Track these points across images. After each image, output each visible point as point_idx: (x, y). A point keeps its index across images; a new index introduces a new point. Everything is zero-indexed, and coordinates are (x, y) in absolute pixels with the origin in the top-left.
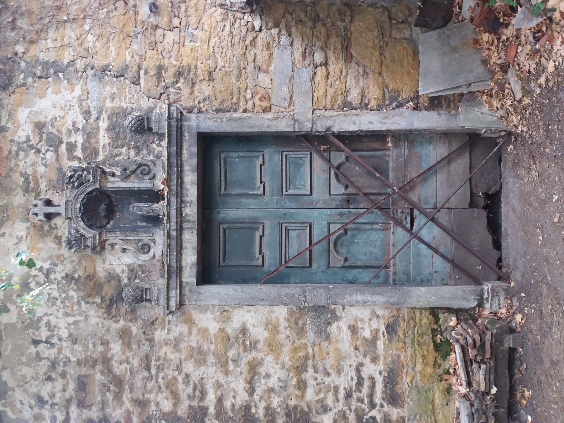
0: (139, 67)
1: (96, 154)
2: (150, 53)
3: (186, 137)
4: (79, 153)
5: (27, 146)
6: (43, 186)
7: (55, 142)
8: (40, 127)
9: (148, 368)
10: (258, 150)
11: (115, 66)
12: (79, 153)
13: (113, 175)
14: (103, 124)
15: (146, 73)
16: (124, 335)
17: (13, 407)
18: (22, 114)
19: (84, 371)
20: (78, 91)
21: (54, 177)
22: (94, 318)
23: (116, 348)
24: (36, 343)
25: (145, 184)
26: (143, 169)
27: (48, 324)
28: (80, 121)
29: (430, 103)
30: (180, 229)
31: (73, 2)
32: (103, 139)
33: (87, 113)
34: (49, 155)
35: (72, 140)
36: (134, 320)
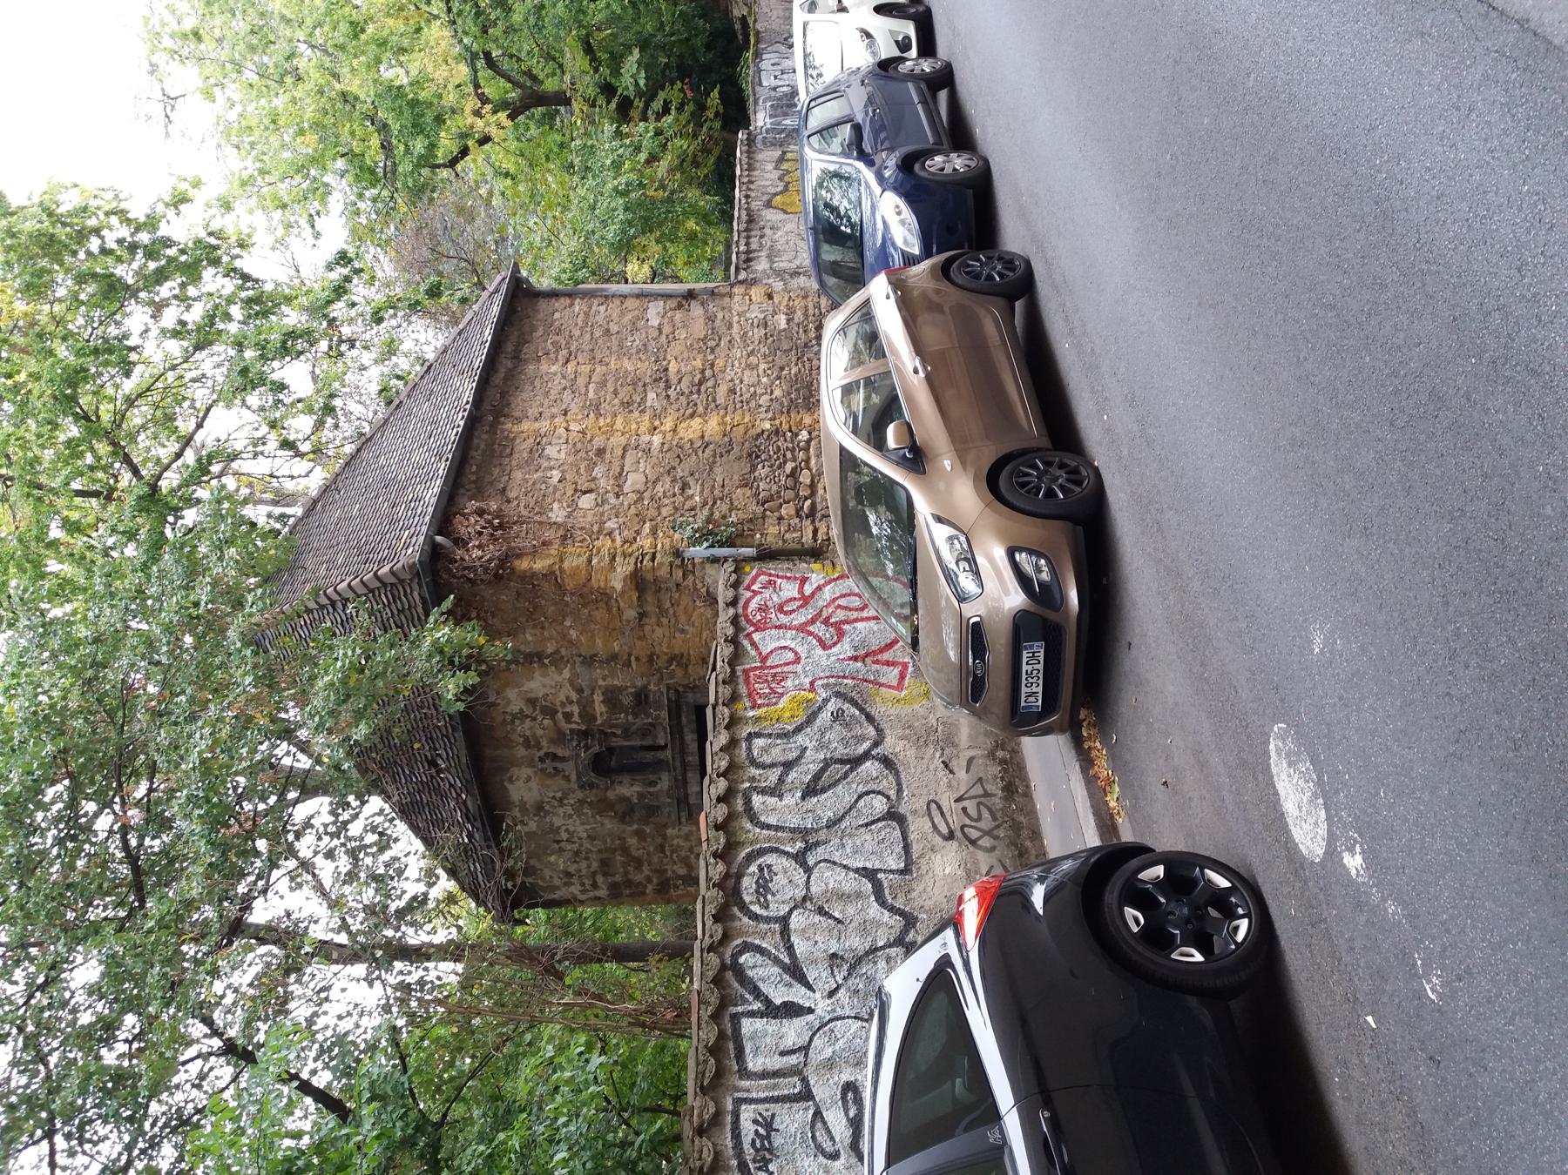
0: (630, 655)
1: (595, 719)
2: (639, 643)
3: (684, 708)
4: (576, 718)
5: (522, 715)
6: (544, 743)
7: (550, 712)
8: (532, 702)
9: (663, 851)
10: (949, 394)
11: (603, 655)
12: (576, 718)
13: (614, 734)
14: (598, 697)
15: (637, 659)
16: (640, 835)
17: (543, 879)
18: (511, 694)
19: (605, 856)
20: (566, 673)
21: (554, 735)
22: (610, 824)
23: (633, 841)
24: (558, 842)
25: (648, 742)
26: (647, 731)
27: (567, 831)
28: (574, 696)
29: (487, 634)
30: (684, 772)
31: (4, 460)
32: (599, 708)
33: (580, 691)
34: (546, 722)
35: (568, 709)
36: (647, 824)
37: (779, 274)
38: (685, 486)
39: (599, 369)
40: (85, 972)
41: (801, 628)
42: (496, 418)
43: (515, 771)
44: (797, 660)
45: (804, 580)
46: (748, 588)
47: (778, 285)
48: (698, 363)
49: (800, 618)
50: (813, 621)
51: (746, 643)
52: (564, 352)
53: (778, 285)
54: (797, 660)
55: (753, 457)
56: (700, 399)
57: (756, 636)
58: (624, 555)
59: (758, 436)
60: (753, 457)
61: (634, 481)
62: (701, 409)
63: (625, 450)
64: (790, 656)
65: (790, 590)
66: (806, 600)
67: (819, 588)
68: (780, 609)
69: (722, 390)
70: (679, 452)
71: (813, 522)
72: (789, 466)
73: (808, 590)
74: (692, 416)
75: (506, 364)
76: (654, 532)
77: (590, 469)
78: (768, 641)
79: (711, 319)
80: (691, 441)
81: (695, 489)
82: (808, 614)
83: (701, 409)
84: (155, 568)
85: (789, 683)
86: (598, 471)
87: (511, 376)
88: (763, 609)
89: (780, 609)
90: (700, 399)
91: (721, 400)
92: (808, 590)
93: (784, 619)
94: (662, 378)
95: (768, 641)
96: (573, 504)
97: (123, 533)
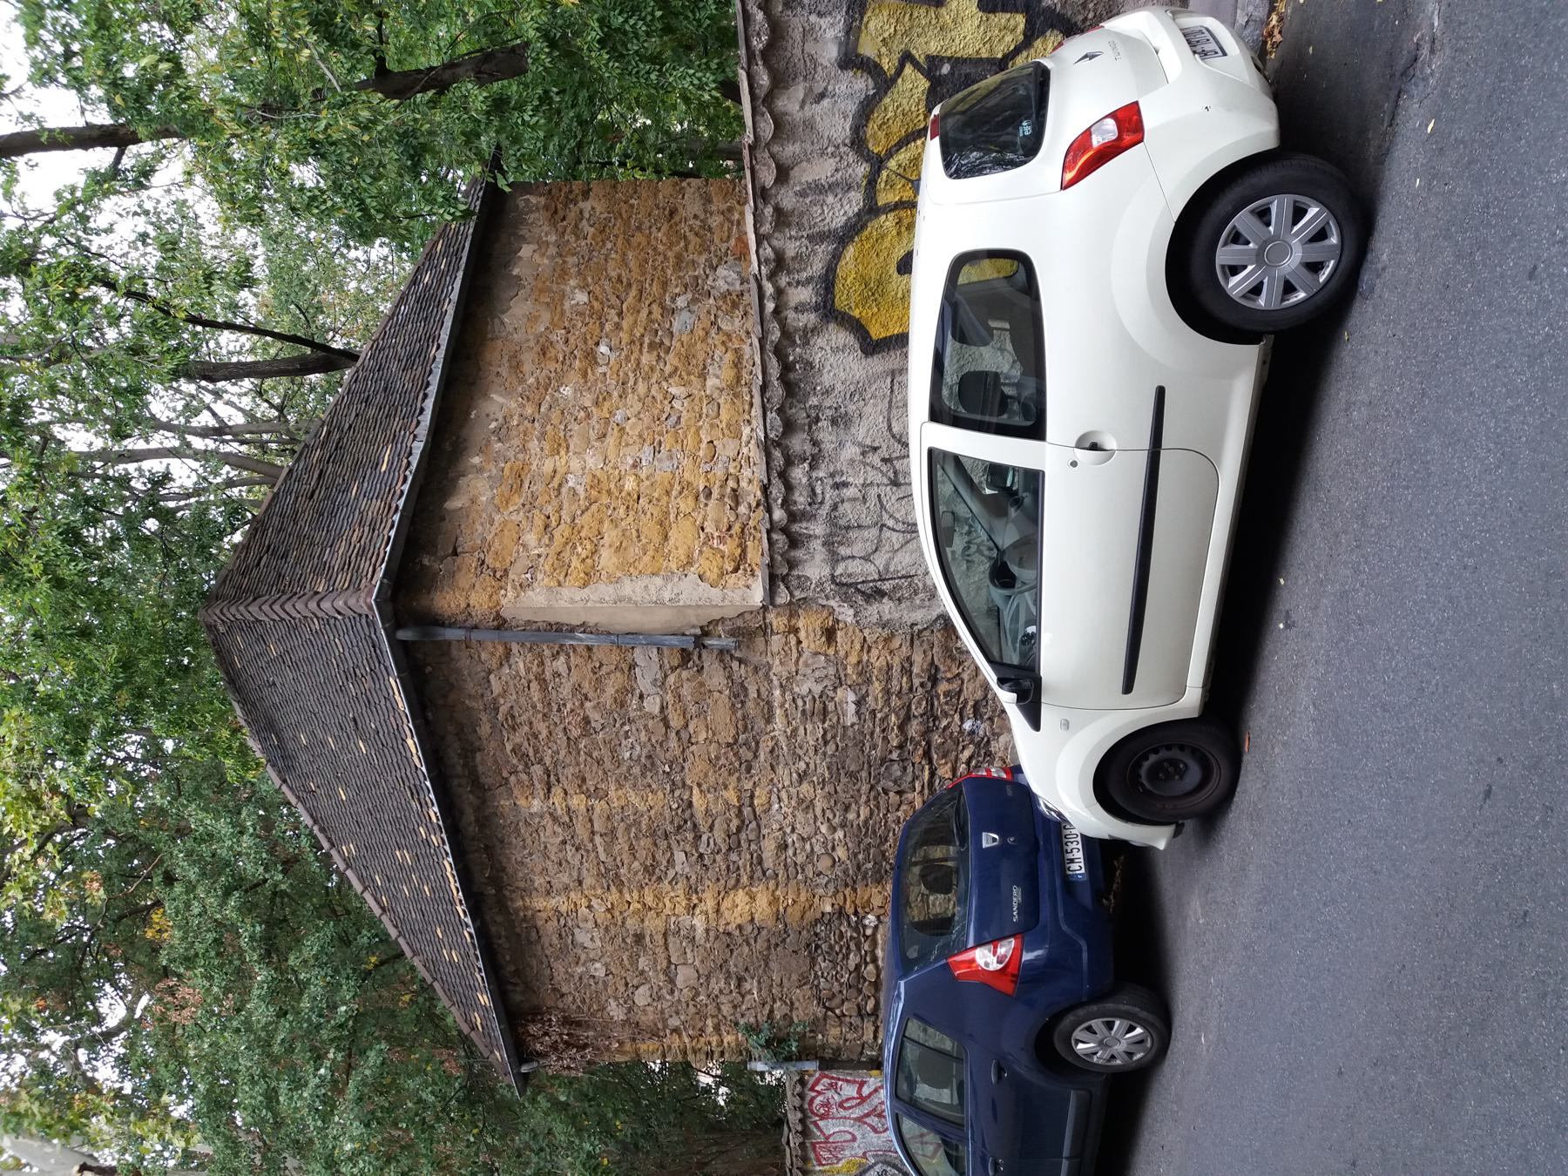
37: (846, 588)
38: (740, 980)
39: (599, 806)
40: (70, 868)
41: (860, 1120)
42: (491, 856)
43: (531, 217)
44: (854, 1139)
45: (862, 1084)
46: (812, 1089)
47: (846, 614)
48: (731, 796)
49: (857, 1113)
50: (867, 1115)
51: (812, 1127)
52: (537, 770)
53: (846, 614)
54: (854, 1139)
55: (812, 949)
56: (742, 860)
57: (821, 1123)
58: (695, 1052)
59: (817, 921)
60: (812, 949)
61: (684, 976)
62: (744, 879)
63: (665, 935)
64: (849, 1137)
65: (850, 1091)
66: (863, 1099)
67: (876, 1090)
68: (841, 1105)
69: (769, 846)
70: (728, 939)
71: (874, 1023)
72: (853, 960)
73: (866, 1091)
74: (735, 887)
75: (467, 799)
76: (717, 1028)
77: (634, 959)
78: (830, 1127)
79: (739, 693)
80: (740, 927)
81: (751, 985)
82: (866, 1108)
83: (744, 879)
84: (15, 742)
85: (847, 1153)
86: (643, 963)
87: (486, 821)
88: (827, 1104)
89: (841, 1105)
90: (742, 860)
91: (769, 863)
92: (866, 1091)
93: (843, 1113)
94: (685, 822)
95: (830, 1127)
96: (630, 999)
97: (29, 791)
